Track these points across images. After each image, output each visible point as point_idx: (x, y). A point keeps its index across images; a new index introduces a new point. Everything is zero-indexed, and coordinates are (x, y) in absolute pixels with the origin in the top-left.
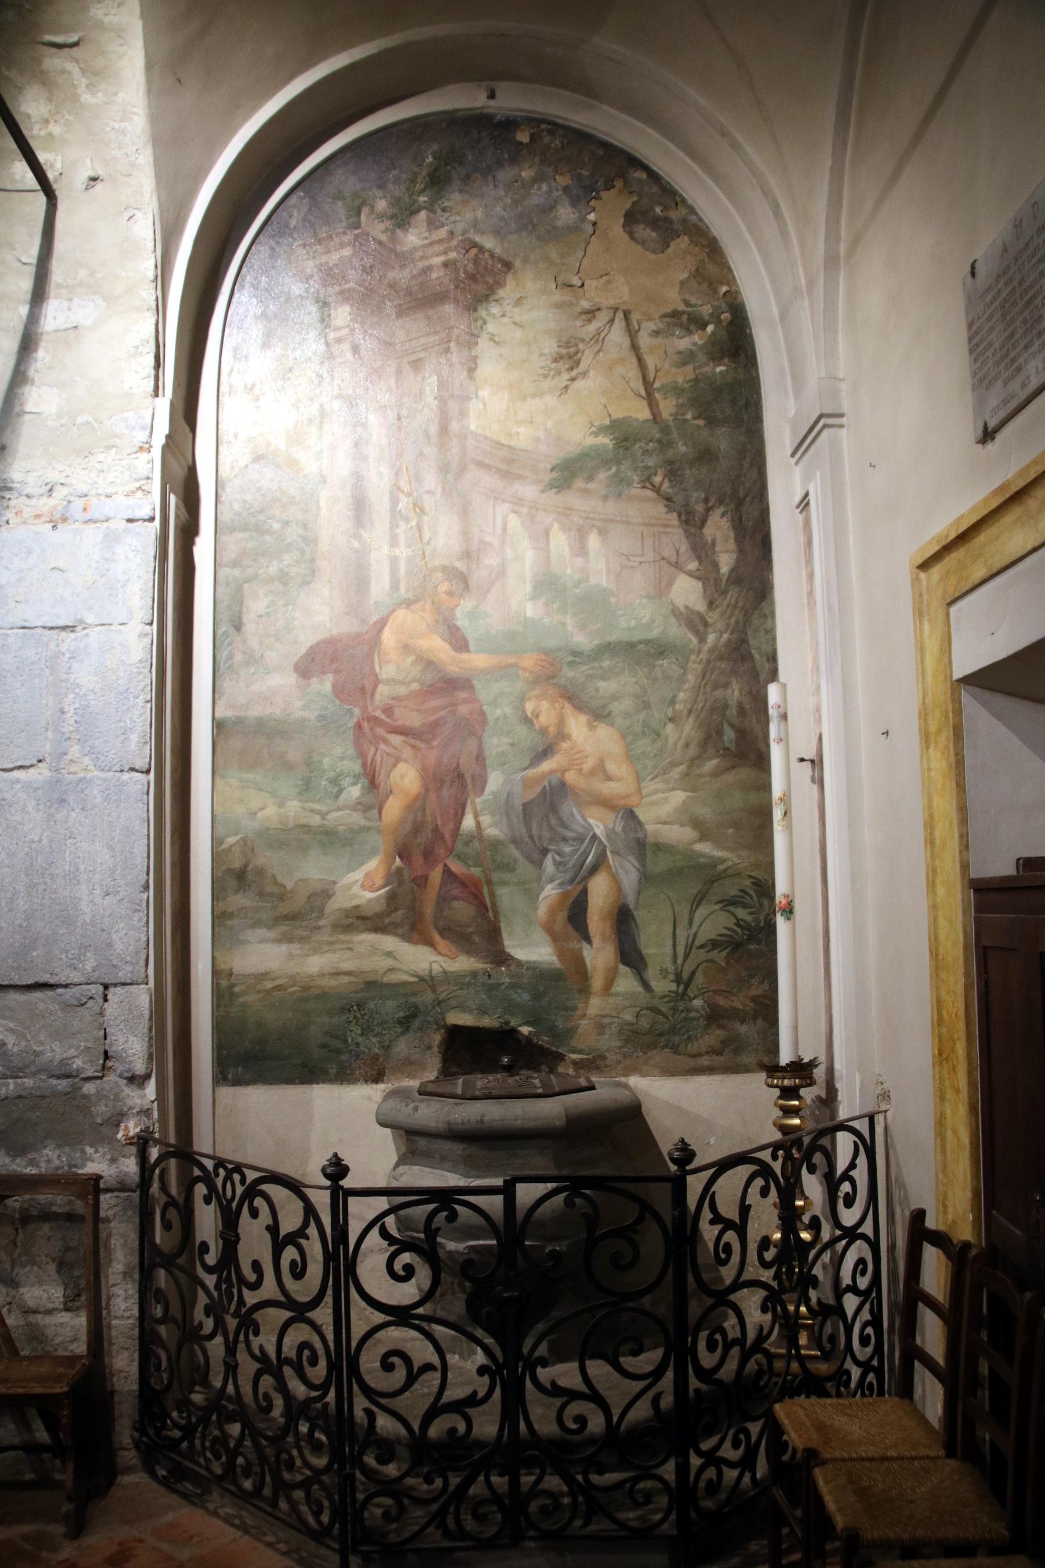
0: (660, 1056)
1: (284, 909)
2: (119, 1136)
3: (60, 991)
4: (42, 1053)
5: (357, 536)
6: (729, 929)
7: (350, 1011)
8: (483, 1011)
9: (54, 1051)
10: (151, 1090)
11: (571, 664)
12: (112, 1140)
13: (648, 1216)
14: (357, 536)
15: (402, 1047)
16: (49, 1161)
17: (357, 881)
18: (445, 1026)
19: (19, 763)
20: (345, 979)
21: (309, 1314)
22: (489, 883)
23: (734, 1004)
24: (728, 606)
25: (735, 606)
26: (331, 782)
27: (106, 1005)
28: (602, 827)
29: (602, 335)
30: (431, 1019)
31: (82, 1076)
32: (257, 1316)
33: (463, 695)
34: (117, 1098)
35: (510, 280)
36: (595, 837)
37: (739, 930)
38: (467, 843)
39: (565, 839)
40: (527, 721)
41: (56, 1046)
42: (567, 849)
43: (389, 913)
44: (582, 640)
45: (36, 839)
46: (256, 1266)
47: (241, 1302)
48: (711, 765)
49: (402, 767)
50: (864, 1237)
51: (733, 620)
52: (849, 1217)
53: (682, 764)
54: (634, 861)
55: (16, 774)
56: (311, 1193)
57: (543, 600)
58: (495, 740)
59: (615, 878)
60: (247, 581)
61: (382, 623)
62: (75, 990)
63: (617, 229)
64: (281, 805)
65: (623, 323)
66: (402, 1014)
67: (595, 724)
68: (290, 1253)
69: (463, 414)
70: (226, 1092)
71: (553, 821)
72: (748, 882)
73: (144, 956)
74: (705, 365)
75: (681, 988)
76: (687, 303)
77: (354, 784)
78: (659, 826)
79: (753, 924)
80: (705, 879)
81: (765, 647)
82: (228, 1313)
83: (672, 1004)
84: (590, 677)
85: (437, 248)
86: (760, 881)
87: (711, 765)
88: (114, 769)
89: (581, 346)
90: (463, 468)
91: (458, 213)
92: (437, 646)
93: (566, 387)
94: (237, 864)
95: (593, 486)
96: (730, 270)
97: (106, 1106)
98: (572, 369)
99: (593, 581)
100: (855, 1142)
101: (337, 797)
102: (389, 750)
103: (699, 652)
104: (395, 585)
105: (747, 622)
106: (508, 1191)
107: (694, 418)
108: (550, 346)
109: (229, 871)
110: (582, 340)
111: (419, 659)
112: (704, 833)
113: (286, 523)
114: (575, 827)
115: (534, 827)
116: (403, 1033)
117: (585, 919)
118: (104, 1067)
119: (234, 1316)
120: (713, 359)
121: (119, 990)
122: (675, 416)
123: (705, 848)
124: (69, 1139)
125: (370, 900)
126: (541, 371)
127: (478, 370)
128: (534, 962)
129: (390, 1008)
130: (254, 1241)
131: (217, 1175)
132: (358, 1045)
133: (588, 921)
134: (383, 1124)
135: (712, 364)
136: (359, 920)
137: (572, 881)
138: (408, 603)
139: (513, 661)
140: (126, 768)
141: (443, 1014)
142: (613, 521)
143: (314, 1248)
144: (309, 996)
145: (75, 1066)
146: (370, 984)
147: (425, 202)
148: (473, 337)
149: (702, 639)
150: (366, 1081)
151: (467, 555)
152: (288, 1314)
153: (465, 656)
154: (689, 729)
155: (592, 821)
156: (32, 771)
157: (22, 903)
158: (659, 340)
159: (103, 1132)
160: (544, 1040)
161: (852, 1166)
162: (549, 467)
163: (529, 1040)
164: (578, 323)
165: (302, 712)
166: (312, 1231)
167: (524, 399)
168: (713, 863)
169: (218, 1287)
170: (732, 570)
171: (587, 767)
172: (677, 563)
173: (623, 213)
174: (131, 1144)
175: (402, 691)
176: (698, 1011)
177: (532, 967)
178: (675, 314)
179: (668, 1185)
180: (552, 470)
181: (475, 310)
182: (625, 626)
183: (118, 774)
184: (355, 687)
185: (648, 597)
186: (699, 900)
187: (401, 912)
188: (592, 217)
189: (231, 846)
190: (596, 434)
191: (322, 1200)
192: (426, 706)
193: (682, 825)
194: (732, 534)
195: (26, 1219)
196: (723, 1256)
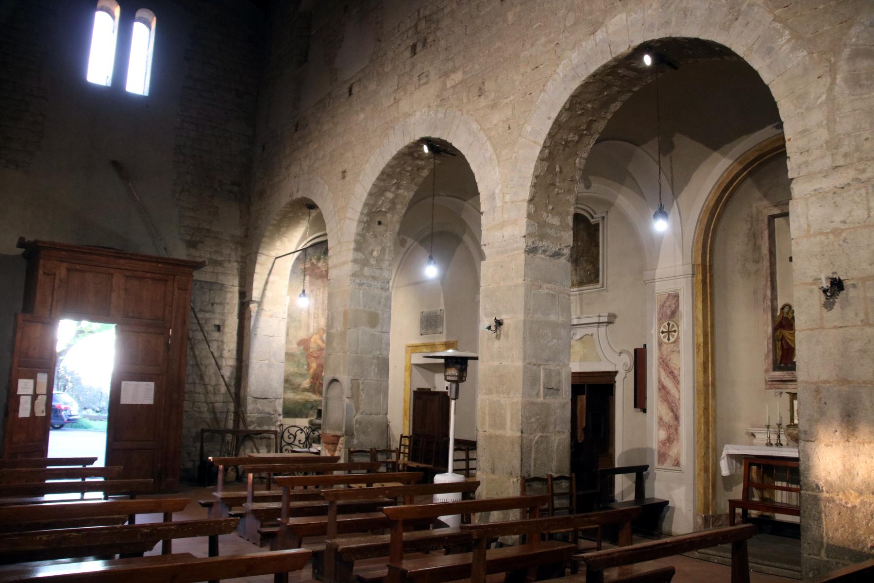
9: (267, 410)
15: (311, 412)
124: (268, 425)
129: (309, 406)
144: (296, 403)
159: (274, 424)
184: (307, 349)
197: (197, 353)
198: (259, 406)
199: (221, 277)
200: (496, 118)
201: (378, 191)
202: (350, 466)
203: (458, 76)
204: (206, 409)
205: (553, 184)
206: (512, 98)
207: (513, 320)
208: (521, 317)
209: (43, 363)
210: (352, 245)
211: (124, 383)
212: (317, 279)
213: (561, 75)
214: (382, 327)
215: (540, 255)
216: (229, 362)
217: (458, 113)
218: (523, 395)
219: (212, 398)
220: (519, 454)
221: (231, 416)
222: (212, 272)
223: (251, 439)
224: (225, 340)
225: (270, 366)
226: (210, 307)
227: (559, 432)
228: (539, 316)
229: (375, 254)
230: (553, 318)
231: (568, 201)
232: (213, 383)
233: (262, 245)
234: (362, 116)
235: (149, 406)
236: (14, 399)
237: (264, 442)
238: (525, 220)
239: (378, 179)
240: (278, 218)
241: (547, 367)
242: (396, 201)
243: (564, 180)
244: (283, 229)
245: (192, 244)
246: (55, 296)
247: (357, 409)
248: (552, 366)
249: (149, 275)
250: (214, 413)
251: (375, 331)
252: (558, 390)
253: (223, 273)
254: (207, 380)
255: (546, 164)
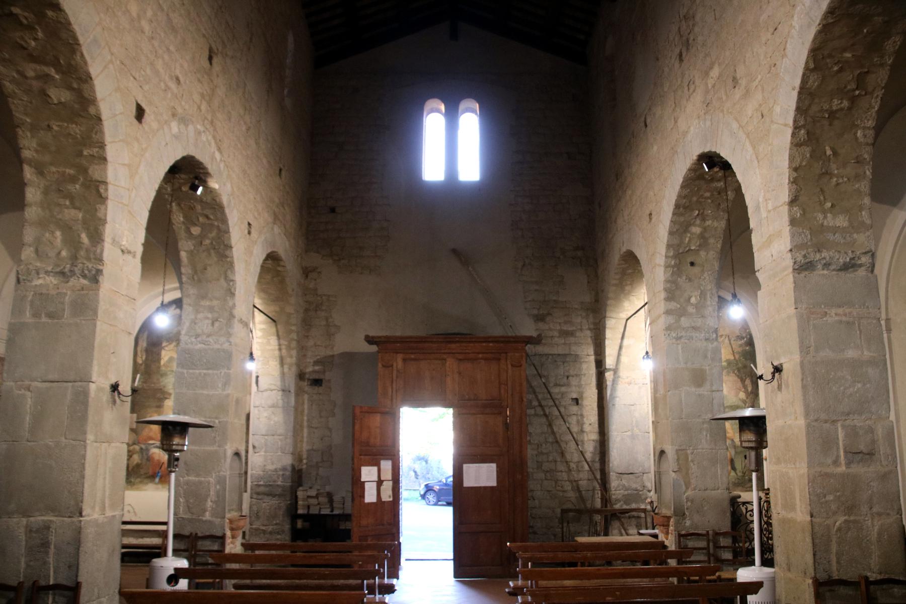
9: (634, 486)
124: (636, 502)
195: (629, 517)
197: (555, 429)
198: (624, 482)
199: (573, 348)
200: (750, 108)
201: (679, 229)
202: (682, 554)
203: (715, 72)
204: (570, 488)
205: (827, 174)
206: (759, 77)
207: (791, 362)
208: (797, 358)
209: (385, 450)
210: (663, 295)
211: (465, 466)
213: (797, 27)
214: (712, 385)
215: (820, 271)
216: (591, 436)
217: (721, 115)
218: (810, 466)
219: (575, 476)
220: (811, 545)
221: (598, 494)
222: (565, 344)
223: (619, 519)
224: (585, 414)
225: (633, 437)
226: (565, 380)
227: (879, 514)
228: (827, 353)
229: (693, 300)
230: (851, 354)
231: (858, 191)
232: (576, 459)
233: (608, 308)
234: (655, 148)
235: (492, 488)
236: (358, 486)
237: (634, 522)
238: (788, 228)
239: (674, 214)
240: (617, 277)
241: (848, 422)
242: (707, 235)
243: (844, 165)
244: (627, 288)
245: (540, 318)
246: (394, 386)
247: (688, 485)
248: (857, 421)
249: (480, 356)
250: (580, 492)
251: (704, 391)
252: (871, 454)
253: (575, 343)
254: (568, 457)
255: (807, 150)
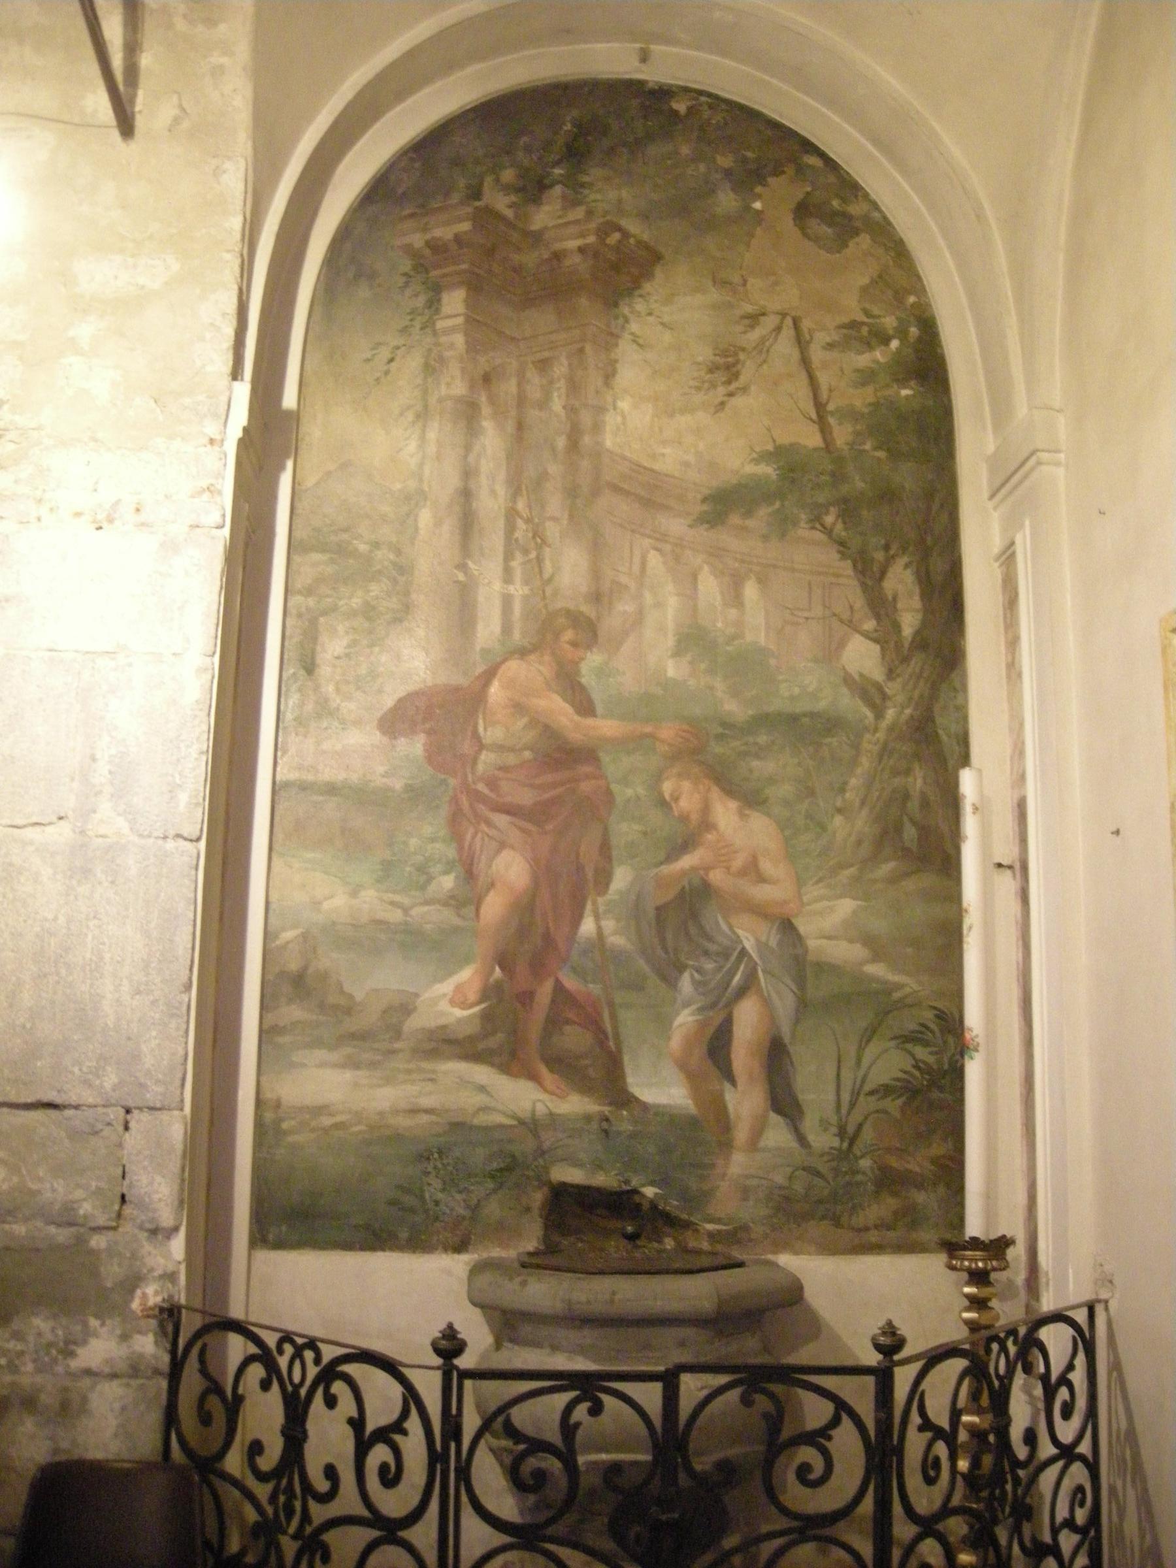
0: (815, 1229)
1: (352, 1024)
2: (135, 1305)
3: (69, 1113)
4: (39, 1192)
5: (462, 567)
6: (905, 1072)
7: (428, 1159)
8: (598, 1166)
10: (178, 1246)
11: (720, 737)
12: (122, 1310)
13: (844, 1417)
14: (462, 567)
16: (39, 1334)
17: (445, 995)
18: (549, 1183)
19: (34, 819)
20: (424, 1119)
21: (401, 1534)
22: (611, 1004)
23: (910, 1167)
24: (911, 676)
25: (919, 677)
26: (418, 870)
27: (127, 1135)
28: (752, 939)
29: (767, 344)
30: (531, 1173)
31: (93, 1224)
32: (329, 1537)
33: (587, 769)
34: (134, 1256)
35: (658, 272)
36: (743, 952)
37: (917, 1073)
38: (585, 952)
39: (706, 953)
40: (663, 804)
41: (60, 1185)
42: (709, 966)
43: (485, 1035)
44: (733, 708)
45: (50, 916)
46: (331, 1472)
47: (306, 1517)
48: (887, 868)
49: (506, 855)
50: (1082, 1458)
51: (917, 693)
52: (1067, 1431)
53: (852, 865)
54: (789, 982)
55: (29, 833)
56: (412, 1375)
57: (688, 657)
58: (624, 827)
59: (766, 1002)
60: (324, 613)
61: (489, 675)
62: (89, 1113)
63: (787, 223)
64: (354, 894)
65: (792, 332)
66: (495, 1165)
67: (747, 812)
68: (380, 1454)
69: (597, 428)
70: (267, 1258)
71: (693, 930)
72: (928, 1016)
73: (180, 1075)
74: (887, 386)
75: (845, 1145)
76: (867, 313)
77: (446, 873)
78: (824, 942)
79: (935, 1067)
80: (882, 1005)
81: (953, 728)
82: (285, 1533)
83: (834, 1164)
84: (744, 755)
85: (572, 230)
86: (943, 1012)
87: (887, 868)
88: (155, 834)
89: (742, 356)
90: (596, 492)
91: (599, 191)
92: (558, 709)
93: (722, 404)
94: (294, 966)
95: (750, 523)
96: (919, 278)
97: (120, 1265)
98: (729, 382)
99: (749, 638)
100: (1074, 1338)
101: (423, 888)
102: (493, 832)
103: (876, 730)
104: (507, 629)
105: (933, 696)
106: (669, 1380)
107: (876, 449)
108: (704, 353)
109: (282, 974)
110: (743, 350)
111: (533, 723)
112: (877, 948)
113: (376, 545)
114: (720, 939)
115: (669, 936)
116: (495, 1191)
117: (728, 1054)
118: (119, 1215)
119: (295, 1537)
120: (897, 380)
121: (145, 1117)
122: (851, 445)
123: (877, 970)
125: (459, 1021)
126: (692, 383)
127: (618, 376)
128: (664, 1106)
130: (328, 1437)
131: (281, 1351)
132: (437, 1203)
133: (733, 1056)
134: (475, 1304)
135: (895, 386)
136: (444, 1044)
137: (713, 1006)
138: (522, 653)
139: (648, 729)
140: (172, 833)
141: (546, 1169)
142: (775, 566)
143: (414, 1445)
144: (383, 1138)
145: (81, 1212)
146: (457, 1126)
147: (561, 175)
148: (611, 338)
149: (879, 715)
150: (446, 1249)
151: (596, 597)
152: (375, 1534)
153: (590, 721)
154: (862, 823)
155: (740, 932)
156: (49, 829)
157: (27, 998)
158: (835, 354)
160: (673, 1205)
161: (1070, 1367)
162: (699, 497)
163: (654, 1206)
164: (740, 328)
165: (385, 780)
166: (414, 1424)
167: (671, 415)
168: (888, 989)
169: (273, 1498)
170: (917, 633)
171: (738, 863)
172: (851, 621)
173: (793, 206)
174: (148, 1316)
175: (511, 759)
176: (864, 1173)
177: (658, 1111)
178: (854, 325)
179: (870, 1380)
180: (705, 500)
181: (616, 305)
182: (787, 694)
183: (160, 842)
185: (816, 660)
186: (869, 1034)
187: (500, 1036)
188: (758, 205)
189: (288, 943)
190: (756, 461)
191: (429, 1386)
192: (537, 781)
193: (851, 941)
194: (917, 590)
196: (932, 1473)
212: (528, 302)
